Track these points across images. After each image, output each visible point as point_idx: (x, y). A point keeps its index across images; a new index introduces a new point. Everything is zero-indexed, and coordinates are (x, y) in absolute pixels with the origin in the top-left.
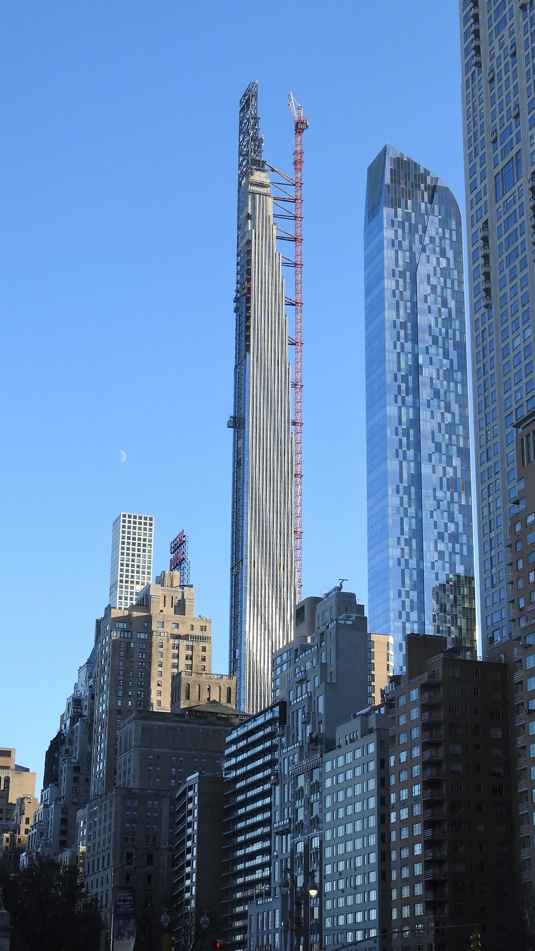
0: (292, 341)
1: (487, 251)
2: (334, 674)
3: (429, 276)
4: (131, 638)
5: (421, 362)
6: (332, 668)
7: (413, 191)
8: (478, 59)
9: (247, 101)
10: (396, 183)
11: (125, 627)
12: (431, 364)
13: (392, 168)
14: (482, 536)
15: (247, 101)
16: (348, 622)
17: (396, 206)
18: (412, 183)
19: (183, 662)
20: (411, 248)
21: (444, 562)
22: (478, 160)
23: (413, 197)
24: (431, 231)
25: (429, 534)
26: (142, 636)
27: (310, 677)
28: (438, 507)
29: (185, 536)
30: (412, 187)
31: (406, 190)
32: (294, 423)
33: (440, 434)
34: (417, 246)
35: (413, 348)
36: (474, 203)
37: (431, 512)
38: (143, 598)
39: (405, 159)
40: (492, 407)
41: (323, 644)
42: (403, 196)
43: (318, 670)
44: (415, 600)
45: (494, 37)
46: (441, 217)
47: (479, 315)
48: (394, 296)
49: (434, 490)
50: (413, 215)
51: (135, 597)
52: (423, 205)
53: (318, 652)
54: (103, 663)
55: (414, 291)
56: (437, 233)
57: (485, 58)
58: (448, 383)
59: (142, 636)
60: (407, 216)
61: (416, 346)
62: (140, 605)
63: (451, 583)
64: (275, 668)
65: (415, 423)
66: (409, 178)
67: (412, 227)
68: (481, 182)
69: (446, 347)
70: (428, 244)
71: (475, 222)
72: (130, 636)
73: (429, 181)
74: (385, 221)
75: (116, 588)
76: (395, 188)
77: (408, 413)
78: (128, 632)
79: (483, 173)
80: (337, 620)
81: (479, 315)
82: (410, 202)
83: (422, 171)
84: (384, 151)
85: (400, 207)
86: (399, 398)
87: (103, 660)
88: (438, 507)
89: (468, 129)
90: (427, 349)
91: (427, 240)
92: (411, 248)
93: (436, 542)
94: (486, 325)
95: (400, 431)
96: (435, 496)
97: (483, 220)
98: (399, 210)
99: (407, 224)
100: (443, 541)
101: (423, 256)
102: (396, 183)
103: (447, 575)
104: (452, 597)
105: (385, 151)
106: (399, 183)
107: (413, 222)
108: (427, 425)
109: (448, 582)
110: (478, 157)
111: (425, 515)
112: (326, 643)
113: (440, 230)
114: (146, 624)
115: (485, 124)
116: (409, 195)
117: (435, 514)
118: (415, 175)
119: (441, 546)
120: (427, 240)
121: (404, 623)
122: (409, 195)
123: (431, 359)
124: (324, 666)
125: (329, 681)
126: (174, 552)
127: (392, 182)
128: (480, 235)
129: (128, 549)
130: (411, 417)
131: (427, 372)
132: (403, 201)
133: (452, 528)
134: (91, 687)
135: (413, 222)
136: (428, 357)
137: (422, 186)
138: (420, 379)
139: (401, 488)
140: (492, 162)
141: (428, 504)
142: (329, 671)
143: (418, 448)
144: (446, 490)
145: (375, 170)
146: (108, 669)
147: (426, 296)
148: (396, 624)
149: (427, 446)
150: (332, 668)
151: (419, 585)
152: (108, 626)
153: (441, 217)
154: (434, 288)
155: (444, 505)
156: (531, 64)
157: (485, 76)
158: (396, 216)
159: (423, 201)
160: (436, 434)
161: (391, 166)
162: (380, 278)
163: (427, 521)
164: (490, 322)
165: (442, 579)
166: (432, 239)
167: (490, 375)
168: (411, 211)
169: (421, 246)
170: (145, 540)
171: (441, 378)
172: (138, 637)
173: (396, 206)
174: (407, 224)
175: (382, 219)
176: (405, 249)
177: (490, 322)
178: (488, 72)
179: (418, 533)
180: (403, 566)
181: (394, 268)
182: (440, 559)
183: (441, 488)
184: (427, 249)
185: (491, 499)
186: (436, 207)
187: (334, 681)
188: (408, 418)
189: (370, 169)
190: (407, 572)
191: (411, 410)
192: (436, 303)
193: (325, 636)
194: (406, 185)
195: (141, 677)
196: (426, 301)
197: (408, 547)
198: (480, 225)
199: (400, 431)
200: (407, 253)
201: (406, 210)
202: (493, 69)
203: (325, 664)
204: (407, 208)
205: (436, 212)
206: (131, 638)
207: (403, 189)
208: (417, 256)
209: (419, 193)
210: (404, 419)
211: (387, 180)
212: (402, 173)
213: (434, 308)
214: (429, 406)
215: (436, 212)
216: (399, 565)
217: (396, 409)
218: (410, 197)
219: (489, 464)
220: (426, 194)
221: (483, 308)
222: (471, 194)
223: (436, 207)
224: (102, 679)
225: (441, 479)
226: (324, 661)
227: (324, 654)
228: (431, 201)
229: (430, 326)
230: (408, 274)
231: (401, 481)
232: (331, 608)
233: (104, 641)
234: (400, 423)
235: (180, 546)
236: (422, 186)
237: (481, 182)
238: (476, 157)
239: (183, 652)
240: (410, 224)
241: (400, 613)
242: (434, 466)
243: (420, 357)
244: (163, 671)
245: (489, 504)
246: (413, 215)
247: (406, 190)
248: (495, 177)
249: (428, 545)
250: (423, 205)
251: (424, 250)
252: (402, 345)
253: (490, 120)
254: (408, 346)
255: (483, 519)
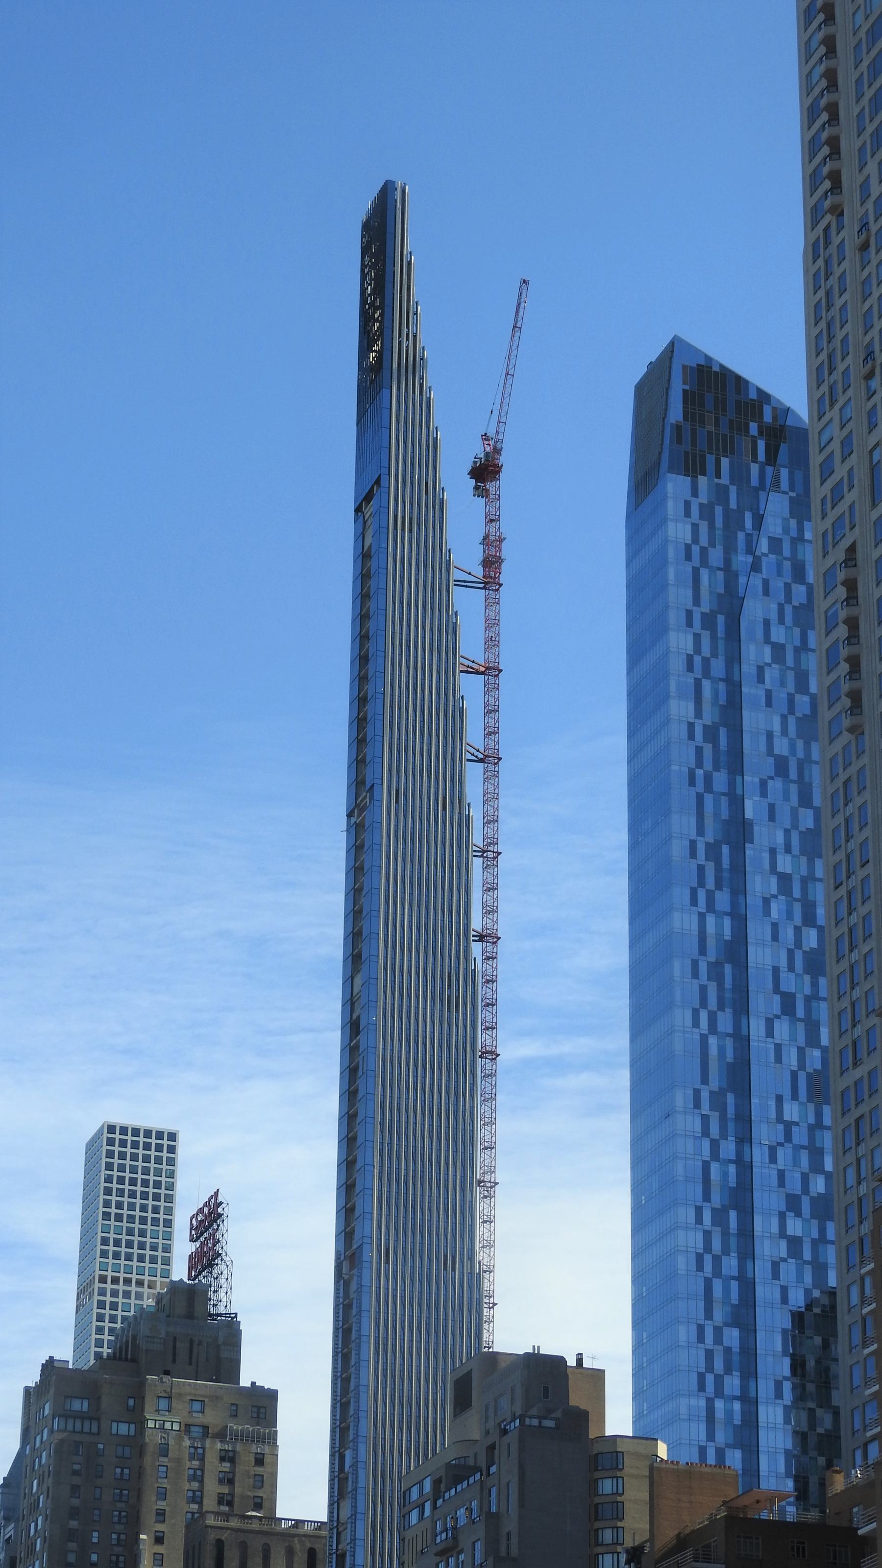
0: (476, 753)
1: (854, 611)
2: (514, 1540)
3: (767, 624)
4: (98, 1434)
5: (749, 814)
6: (511, 1524)
7: (732, 438)
8: (837, 199)
9: (380, 234)
10: (696, 418)
11: (85, 1409)
12: (772, 817)
13: (687, 387)
14: (843, 1231)
15: (380, 234)
16: (549, 1423)
17: (695, 471)
18: (731, 422)
19: (212, 1488)
20: (727, 562)
21: (789, 899)
22: (835, 412)
23: (732, 453)
24: (773, 525)
25: (767, 1201)
26: (123, 1429)
27: (465, 1542)
28: (788, 1137)
29: (221, 1203)
30: (731, 428)
31: (717, 435)
32: (481, 938)
33: (792, 976)
34: (742, 560)
35: (732, 784)
36: (829, 506)
37: (773, 1150)
38: (127, 1342)
39: (716, 369)
40: (865, 949)
41: (493, 1469)
42: (710, 447)
43: (480, 1531)
44: (736, 1349)
45: (869, 155)
46: (793, 494)
47: (838, 745)
48: (690, 667)
49: (779, 1099)
50: (733, 490)
51: (106, 1337)
52: (755, 468)
53: (482, 1488)
54: (35, 1490)
55: (734, 658)
56: (786, 530)
57: (850, 197)
58: (807, 745)
59: (123, 1429)
60: (721, 494)
61: (739, 779)
62: (120, 1359)
63: (817, 1310)
64: (406, 1509)
65: (736, 950)
66: (724, 410)
67: (730, 523)
68: (843, 462)
69: (807, 779)
70: (766, 555)
71: (830, 547)
72: (95, 1429)
73: (768, 417)
74: (670, 504)
75: (91, 1295)
76: (694, 432)
77: (719, 927)
78: (91, 1419)
79: (846, 443)
80: (522, 1418)
81: (838, 745)
82: (725, 462)
83: (753, 395)
84: (672, 344)
85: (704, 474)
86: (701, 895)
87: (35, 1483)
88: (788, 1137)
89: (815, 346)
90: (763, 784)
91: (764, 546)
92: (727, 562)
93: (782, 1216)
94: (853, 770)
95: (703, 967)
96: (780, 1118)
97: (846, 543)
98: (702, 480)
99: (719, 510)
100: (798, 1214)
101: (756, 581)
102: (696, 418)
103: (807, 1292)
104: (818, 1340)
105: (672, 352)
106: (702, 423)
107: (733, 505)
108: (761, 956)
109: (809, 1307)
110: (837, 407)
111: (759, 1156)
112: (499, 1468)
113: (793, 523)
114: (131, 1402)
115: (850, 337)
116: (725, 445)
117: (780, 1152)
118: (738, 403)
119: (795, 1227)
120: (764, 546)
121: (710, 1402)
122: (725, 445)
123: (772, 808)
124: (492, 1519)
125: (503, 1553)
126: (198, 1238)
127: (685, 418)
128: (841, 576)
129: (119, 1205)
130: (727, 934)
131: (766, 836)
132: (710, 459)
133: (819, 1185)
134: (8, 1541)
135: (733, 505)
136: (765, 803)
137: (754, 428)
138: (747, 852)
139: (705, 1095)
140: (865, 421)
141: (764, 1133)
142: (504, 1531)
143: (739, 890)
144: (805, 1100)
145: (650, 391)
146: (45, 1502)
147: (760, 670)
148: (693, 1402)
149: (763, 1002)
150: (511, 1524)
151: (744, 1315)
152: (47, 1407)
153: (793, 494)
154: (778, 650)
155: (800, 1136)
156: (825, 352)
157: (849, 236)
158: (695, 493)
159: (755, 459)
160: (783, 975)
161: (684, 383)
162: (660, 629)
163: (763, 1174)
164: (861, 763)
165: (797, 1299)
166: (775, 544)
167: (860, 878)
168: (728, 483)
169: (750, 559)
170: (157, 1184)
171: (796, 849)
172: (114, 1431)
173: (695, 471)
174: (719, 510)
175: (664, 499)
176: (715, 565)
177: (861, 763)
178: (856, 229)
179: (741, 1197)
180: (700, 787)
181: (689, 606)
182: (778, 774)
183: (795, 1096)
184: (764, 564)
185: (862, 1150)
186: (784, 473)
187: (515, 1551)
188: (719, 935)
189: (640, 389)
190: (708, 799)
191: (727, 922)
192: (783, 683)
193: (496, 1452)
194: (717, 425)
195: (119, 1522)
196: (761, 679)
197: (719, 1229)
198: (838, 554)
199: (703, 967)
200: (720, 575)
201: (716, 480)
202: (867, 223)
203: (497, 1515)
204: (718, 476)
205: (785, 484)
206: (98, 1434)
207: (710, 433)
208: (742, 580)
209: (746, 443)
210: (711, 943)
211: (676, 413)
212: (709, 398)
213: (781, 696)
214: (776, 1275)
215: (785, 484)
216: (700, 1267)
217: (695, 919)
218: (725, 450)
219: (860, 1072)
220: (761, 445)
221: (845, 733)
222: (822, 484)
223: (784, 473)
224: (33, 1525)
225: (794, 1075)
226: (494, 1509)
227: (494, 1491)
228: (772, 457)
229: (776, 970)
230: (721, 619)
231: (705, 1080)
232: (513, 1390)
233: (38, 1438)
234: (703, 951)
235: (211, 1225)
236: (754, 428)
237: (843, 462)
238: (832, 405)
239: (214, 1467)
240: (727, 512)
241: (701, 1377)
242: (775, 926)
243: (748, 804)
244: (167, 1509)
245: (858, 1161)
246: (733, 490)
247: (717, 435)
248: (871, 452)
249: (764, 1225)
250: (755, 468)
251: (756, 567)
252: (708, 778)
253: (861, 331)
254: (720, 779)
255: (845, 1192)
